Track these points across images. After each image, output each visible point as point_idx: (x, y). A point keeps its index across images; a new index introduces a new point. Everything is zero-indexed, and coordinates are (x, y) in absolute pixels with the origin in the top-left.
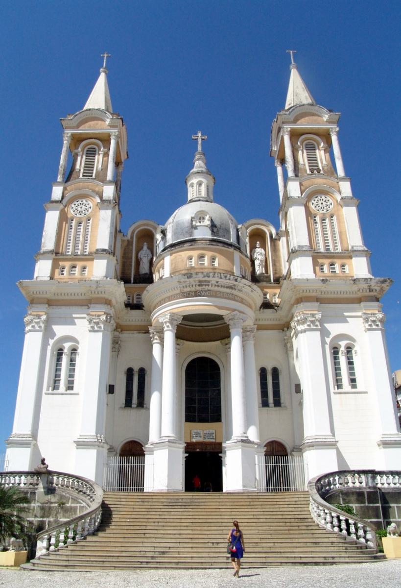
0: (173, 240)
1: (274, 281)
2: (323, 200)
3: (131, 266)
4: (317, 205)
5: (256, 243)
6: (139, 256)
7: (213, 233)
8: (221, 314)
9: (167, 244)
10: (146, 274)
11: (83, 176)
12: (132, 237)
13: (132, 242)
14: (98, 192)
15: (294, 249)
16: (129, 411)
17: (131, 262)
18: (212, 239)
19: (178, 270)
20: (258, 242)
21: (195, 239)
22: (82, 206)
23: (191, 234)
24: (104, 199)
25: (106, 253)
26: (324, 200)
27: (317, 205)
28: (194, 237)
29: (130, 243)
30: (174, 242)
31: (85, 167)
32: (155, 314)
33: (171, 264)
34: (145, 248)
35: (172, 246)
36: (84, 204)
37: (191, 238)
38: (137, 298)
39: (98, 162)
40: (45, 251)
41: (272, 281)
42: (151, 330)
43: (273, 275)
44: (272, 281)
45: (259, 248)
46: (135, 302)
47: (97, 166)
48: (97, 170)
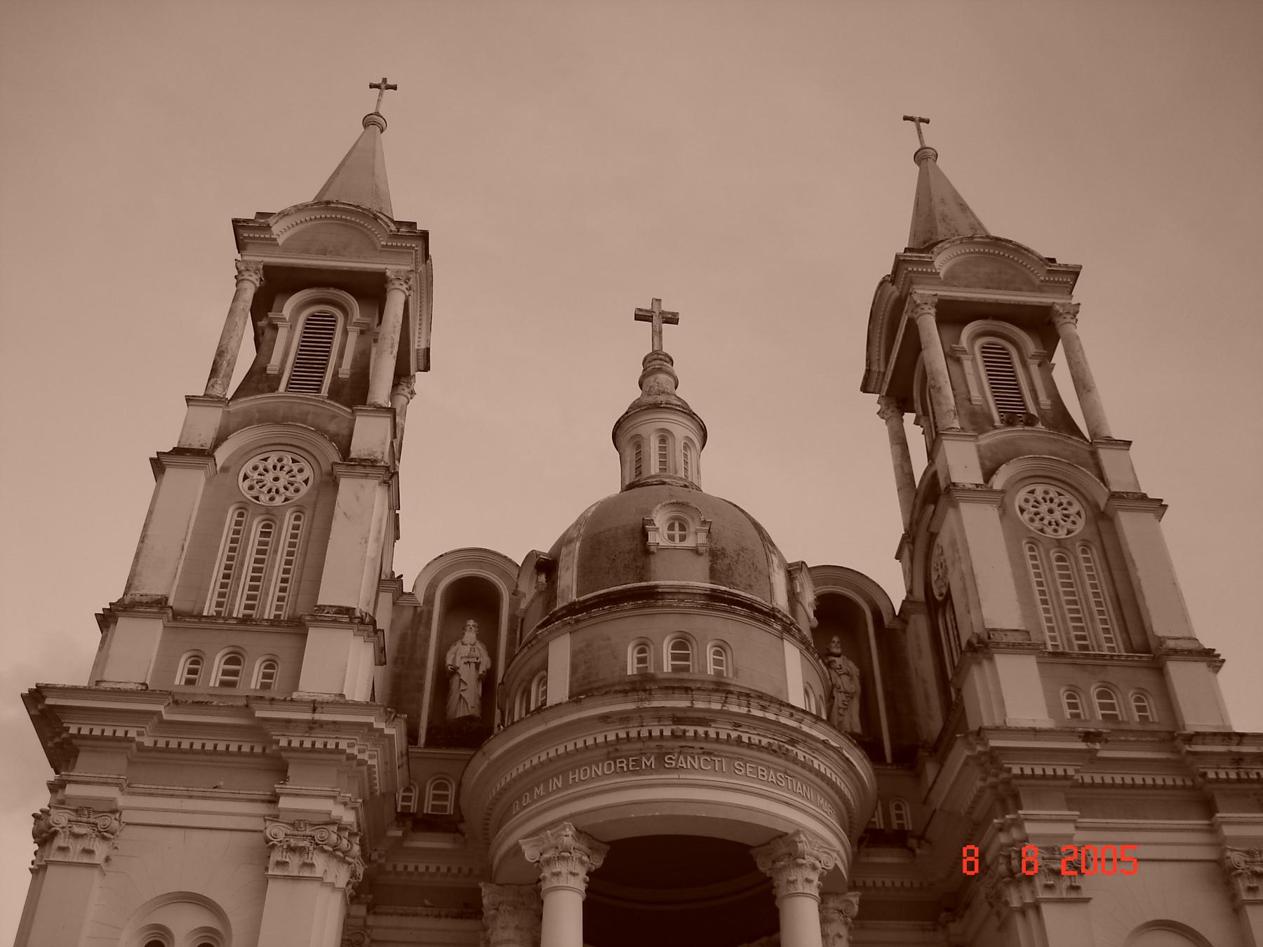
0: (579, 594)
1: (896, 758)
2: (1052, 500)
3: (420, 688)
4: (1037, 514)
5: (830, 641)
6: (449, 661)
7: (714, 575)
8: (746, 842)
9: (560, 604)
10: (470, 718)
11: (288, 388)
12: (429, 600)
13: (430, 613)
14: (337, 435)
15: (975, 641)
16: (985, 663)
17: (422, 677)
18: (713, 590)
19: (598, 684)
20: (836, 639)
21: (656, 587)
22: (278, 473)
23: (643, 573)
24: (353, 455)
25: (351, 622)
26: (1056, 500)
27: (1037, 514)
28: (652, 583)
29: (421, 618)
30: (582, 599)
31: (297, 365)
32: (511, 832)
33: (574, 668)
34: (470, 636)
35: (572, 609)
36: (286, 469)
37: (644, 584)
38: (436, 797)
39: (341, 355)
40: (138, 598)
41: (889, 760)
42: (488, 896)
43: (892, 740)
44: (889, 760)
45: (838, 656)
46: (427, 810)
47: (339, 365)
48: (336, 374)
